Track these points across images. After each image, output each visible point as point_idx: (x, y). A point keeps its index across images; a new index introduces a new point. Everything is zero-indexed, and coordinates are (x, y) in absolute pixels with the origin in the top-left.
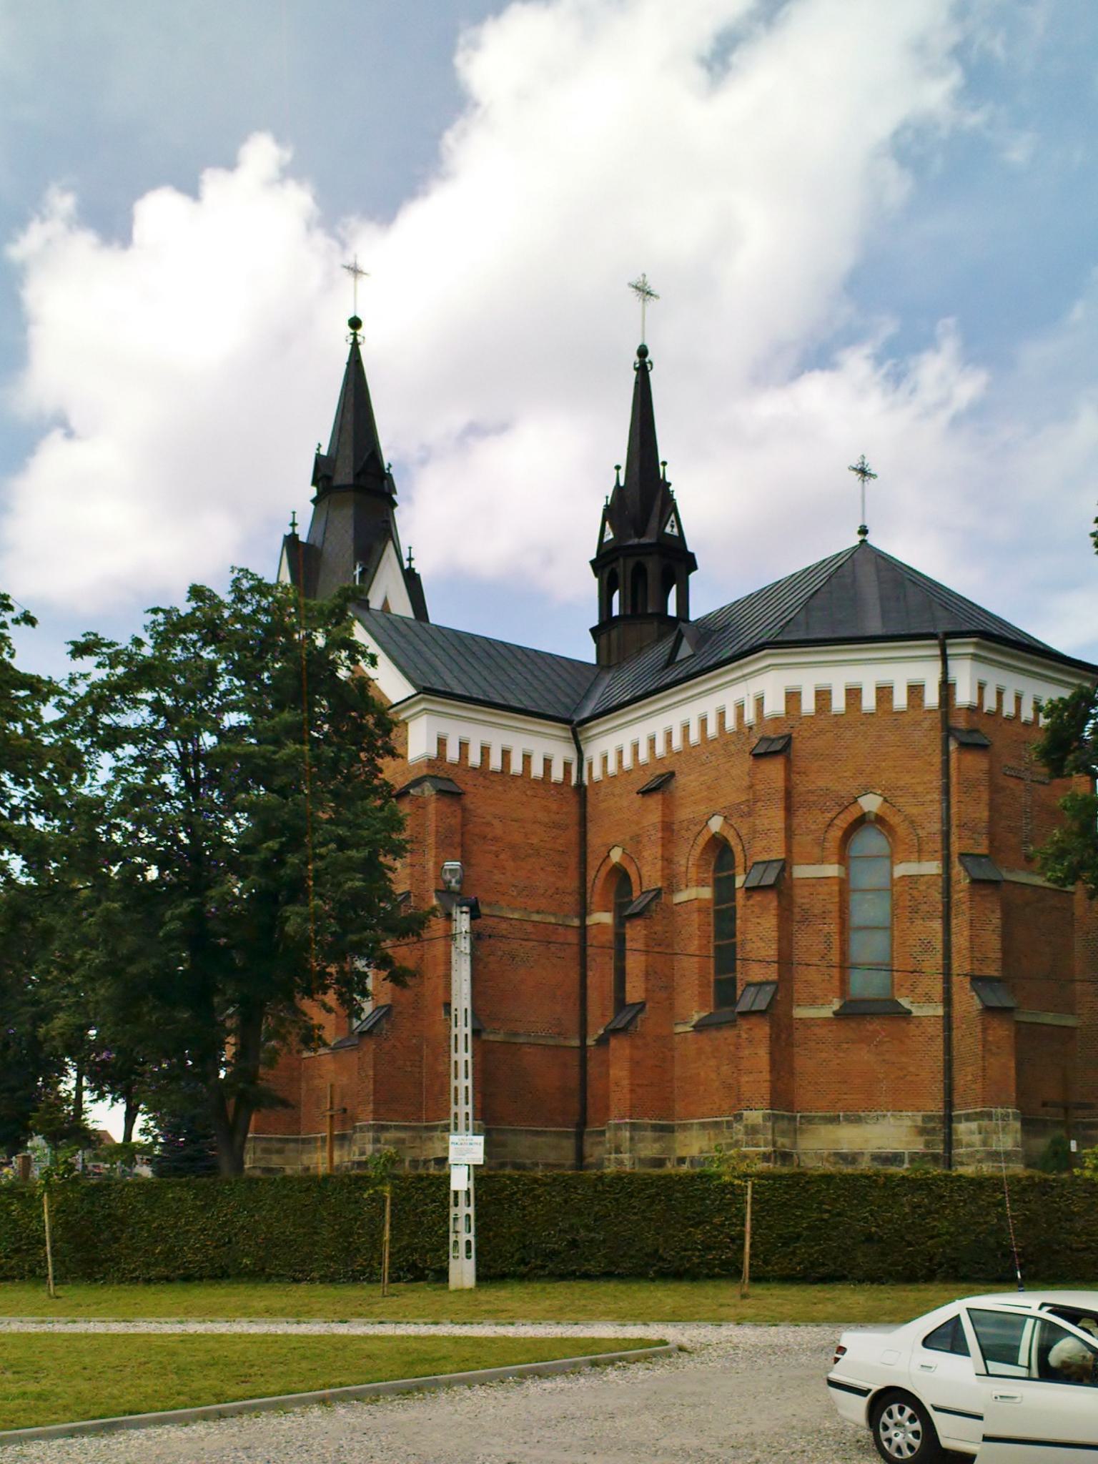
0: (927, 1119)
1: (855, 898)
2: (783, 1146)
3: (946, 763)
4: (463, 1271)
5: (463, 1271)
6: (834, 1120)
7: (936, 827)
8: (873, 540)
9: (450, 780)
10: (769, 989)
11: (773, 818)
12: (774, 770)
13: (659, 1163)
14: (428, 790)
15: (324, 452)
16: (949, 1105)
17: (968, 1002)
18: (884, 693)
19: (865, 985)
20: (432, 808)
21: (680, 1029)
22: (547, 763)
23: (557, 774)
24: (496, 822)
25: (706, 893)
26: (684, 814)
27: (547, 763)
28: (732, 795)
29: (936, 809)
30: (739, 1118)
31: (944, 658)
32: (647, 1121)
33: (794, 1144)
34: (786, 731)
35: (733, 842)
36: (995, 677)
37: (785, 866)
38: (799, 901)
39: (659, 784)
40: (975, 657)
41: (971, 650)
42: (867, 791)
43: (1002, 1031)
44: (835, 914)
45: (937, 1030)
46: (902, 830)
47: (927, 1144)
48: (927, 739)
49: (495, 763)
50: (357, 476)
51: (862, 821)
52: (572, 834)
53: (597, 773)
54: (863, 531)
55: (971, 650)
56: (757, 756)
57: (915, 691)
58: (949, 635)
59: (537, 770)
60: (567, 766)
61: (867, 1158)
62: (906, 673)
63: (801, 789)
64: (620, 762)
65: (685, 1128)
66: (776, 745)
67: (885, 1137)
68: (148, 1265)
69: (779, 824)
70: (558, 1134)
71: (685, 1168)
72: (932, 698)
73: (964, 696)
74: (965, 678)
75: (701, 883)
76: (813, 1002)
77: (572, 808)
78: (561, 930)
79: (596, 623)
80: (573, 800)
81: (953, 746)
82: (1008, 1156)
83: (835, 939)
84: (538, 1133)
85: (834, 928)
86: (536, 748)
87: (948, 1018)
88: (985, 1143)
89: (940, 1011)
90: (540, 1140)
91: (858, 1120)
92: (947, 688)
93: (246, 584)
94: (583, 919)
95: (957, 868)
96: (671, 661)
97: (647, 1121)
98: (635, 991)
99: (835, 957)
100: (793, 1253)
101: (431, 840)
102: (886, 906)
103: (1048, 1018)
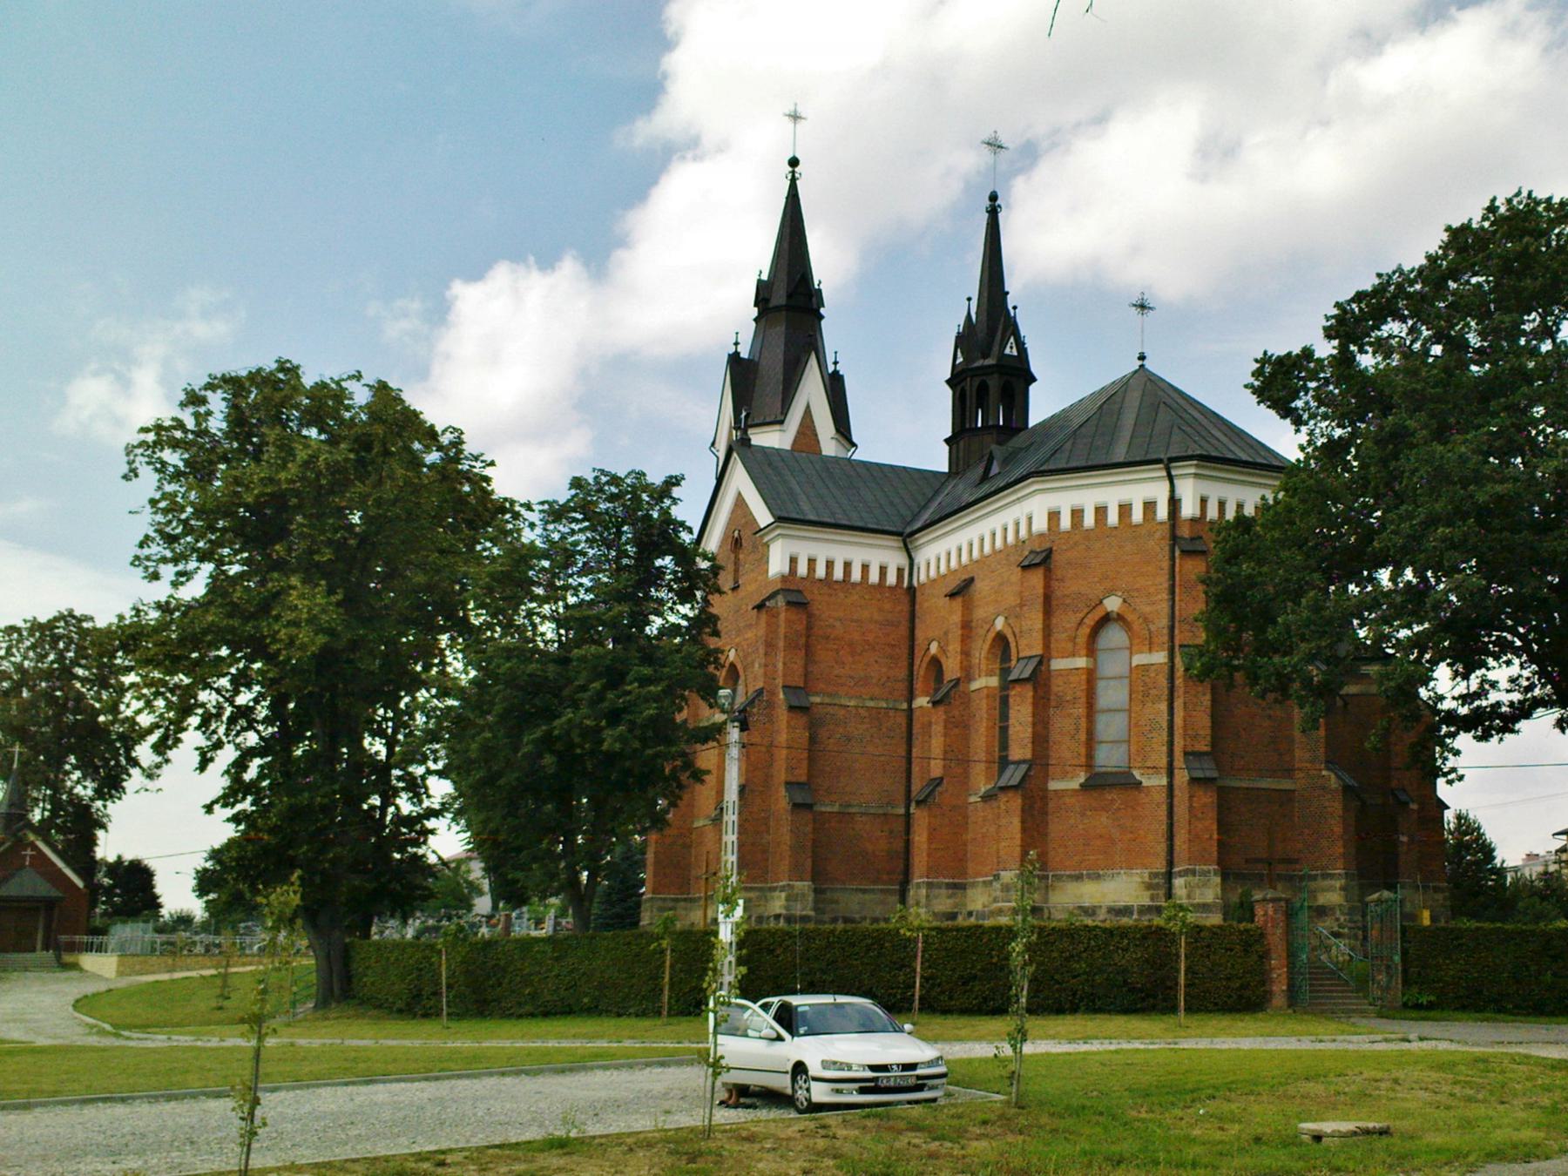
0: (1154, 875)
1: (1101, 685)
3: (1173, 566)
6: (1079, 878)
7: (1165, 622)
8: (1148, 364)
9: (800, 592)
10: (1024, 767)
11: (1035, 620)
12: (1036, 579)
13: (953, 916)
14: (780, 601)
15: (765, 277)
16: (1170, 863)
18: (1125, 510)
19: (1109, 758)
20: (782, 616)
21: (972, 799)
22: (883, 570)
23: (891, 579)
24: (838, 624)
25: (994, 681)
26: (980, 613)
27: (883, 570)
28: (1011, 600)
29: (1164, 607)
30: (997, 877)
31: (1171, 478)
32: (942, 880)
33: (1046, 900)
34: (1048, 545)
35: (1011, 639)
36: (1215, 491)
37: (1043, 660)
38: (1055, 689)
39: (962, 589)
40: (1196, 475)
41: (1193, 470)
42: (1110, 592)
43: (1207, 798)
44: (1084, 700)
45: (1162, 797)
47: (1152, 899)
48: (1159, 547)
49: (838, 574)
50: (790, 296)
51: (1106, 619)
52: (903, 630)
53: (923, 578)
54: (1142, 357)
55: (1193, 470)
56: (1025, 568)
57: (1149, 506)
58: (1172, 460)
59: (874, 577)
60: (900, 571)
61: (1104, 910)
62: (1141, 491)
63: (1058, 593)
64: (1017, 532)
65: (974, 885)
66: (1040, 558)
67: (1115, 892)
68: (520, 1004)
69: (1039, 625)
70: (882, 891)
71: (973, 920)
72: (1162, 512)
73: (1188, 509)
74: (1189, 493)
75: (990, 674)
76: (1064, 776)
77: (904, 607)
78: (892, 713)
79: (949, 434)
80: (906, 600)
81: (1177, 553)
82: (1204, 907)
83: (1083, 723)
84: (864, 891)
85: (1081, 710)
86: (874, 558)
87: (1170, 786)
88: (1189, 897)
89: (1164, 781)
90: (867, 897)
92: (1174, 503)
93: (604, 479)
94: (910, 702)
96: (985, 477)
97: (942, 880)
98: (1020, 749)
99: (1083, 737)
100: (971, 991)
101: (781, 644)
102: (1126, 692)
103: (1266, 783)
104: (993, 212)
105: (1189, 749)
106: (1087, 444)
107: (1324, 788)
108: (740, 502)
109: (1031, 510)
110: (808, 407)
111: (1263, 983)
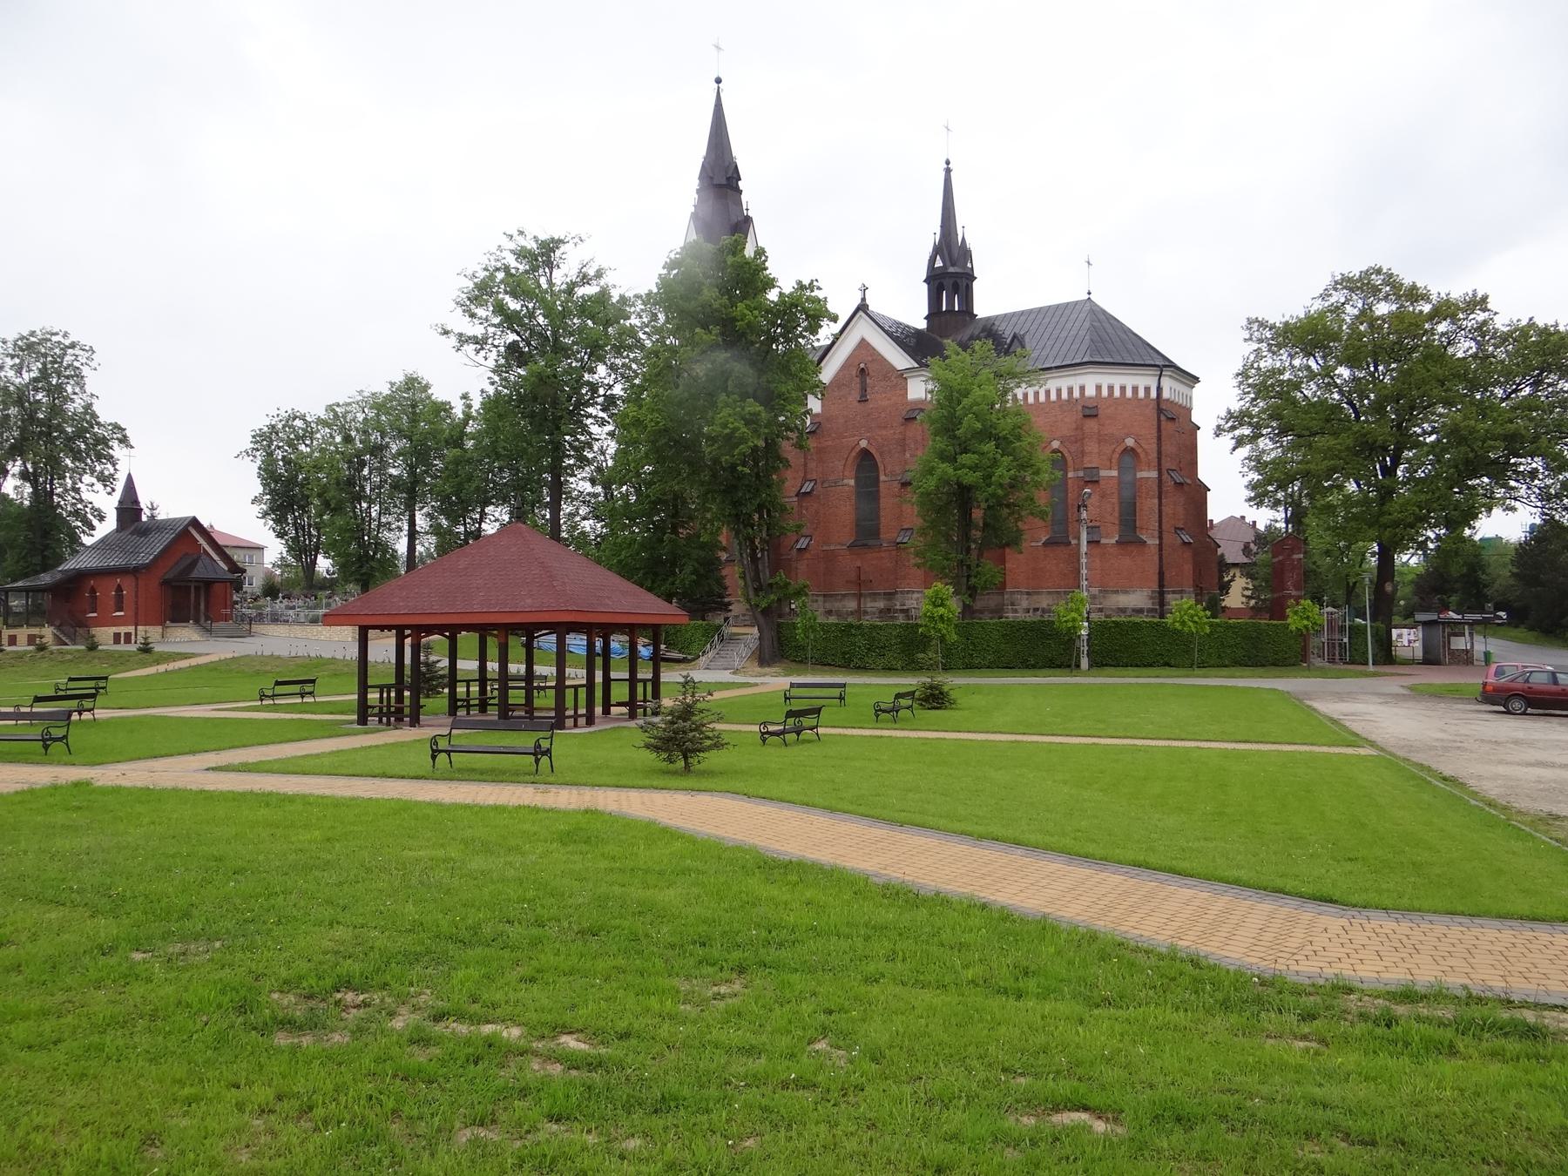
4: (1084, 663)
5: (1084, 663)
6: (1117, 592)
16: (1161, 585)
42: (1128, 435)
45: (1155, 550)
46: (1142, 456)
48: (1152, 413)
57: (1147, 389)
72: (1154, 394)
73: (1166, 394)
87: (1160, 545)
91: (1126, 592)
92: (1159, 389)
111: (385, 551)
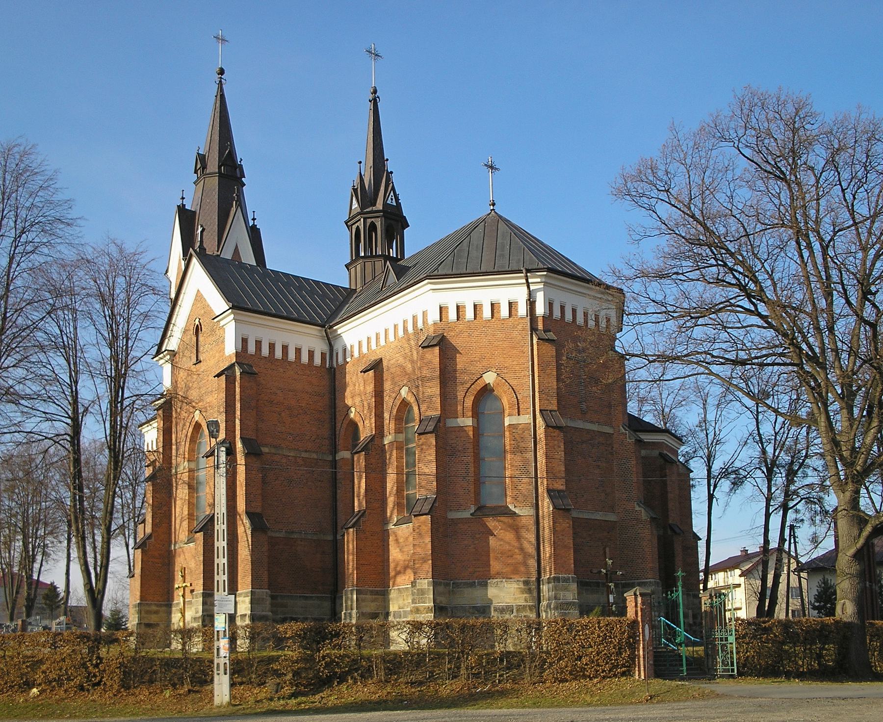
2: (441, 602)
17: (546, 506)
22: (311, 354)
23: (318, 361)
24: (278, 392)
27: (311, 354)
36: (560, 297)
60: (323, 355)
72: (522, 310)
84: (306, 598)
85: (470, 459)
92: (531, 303)
95: (539, 419)
104: (375, 101)
105: (551, 487)
106: (458, 259)
107: (637, 519)
108: (199, 297)
109: (421, 305)
110: (237, 247)
